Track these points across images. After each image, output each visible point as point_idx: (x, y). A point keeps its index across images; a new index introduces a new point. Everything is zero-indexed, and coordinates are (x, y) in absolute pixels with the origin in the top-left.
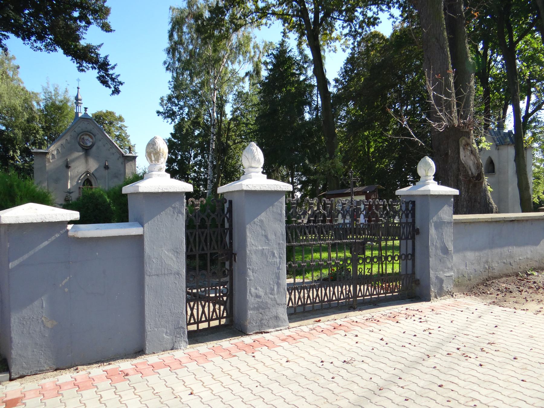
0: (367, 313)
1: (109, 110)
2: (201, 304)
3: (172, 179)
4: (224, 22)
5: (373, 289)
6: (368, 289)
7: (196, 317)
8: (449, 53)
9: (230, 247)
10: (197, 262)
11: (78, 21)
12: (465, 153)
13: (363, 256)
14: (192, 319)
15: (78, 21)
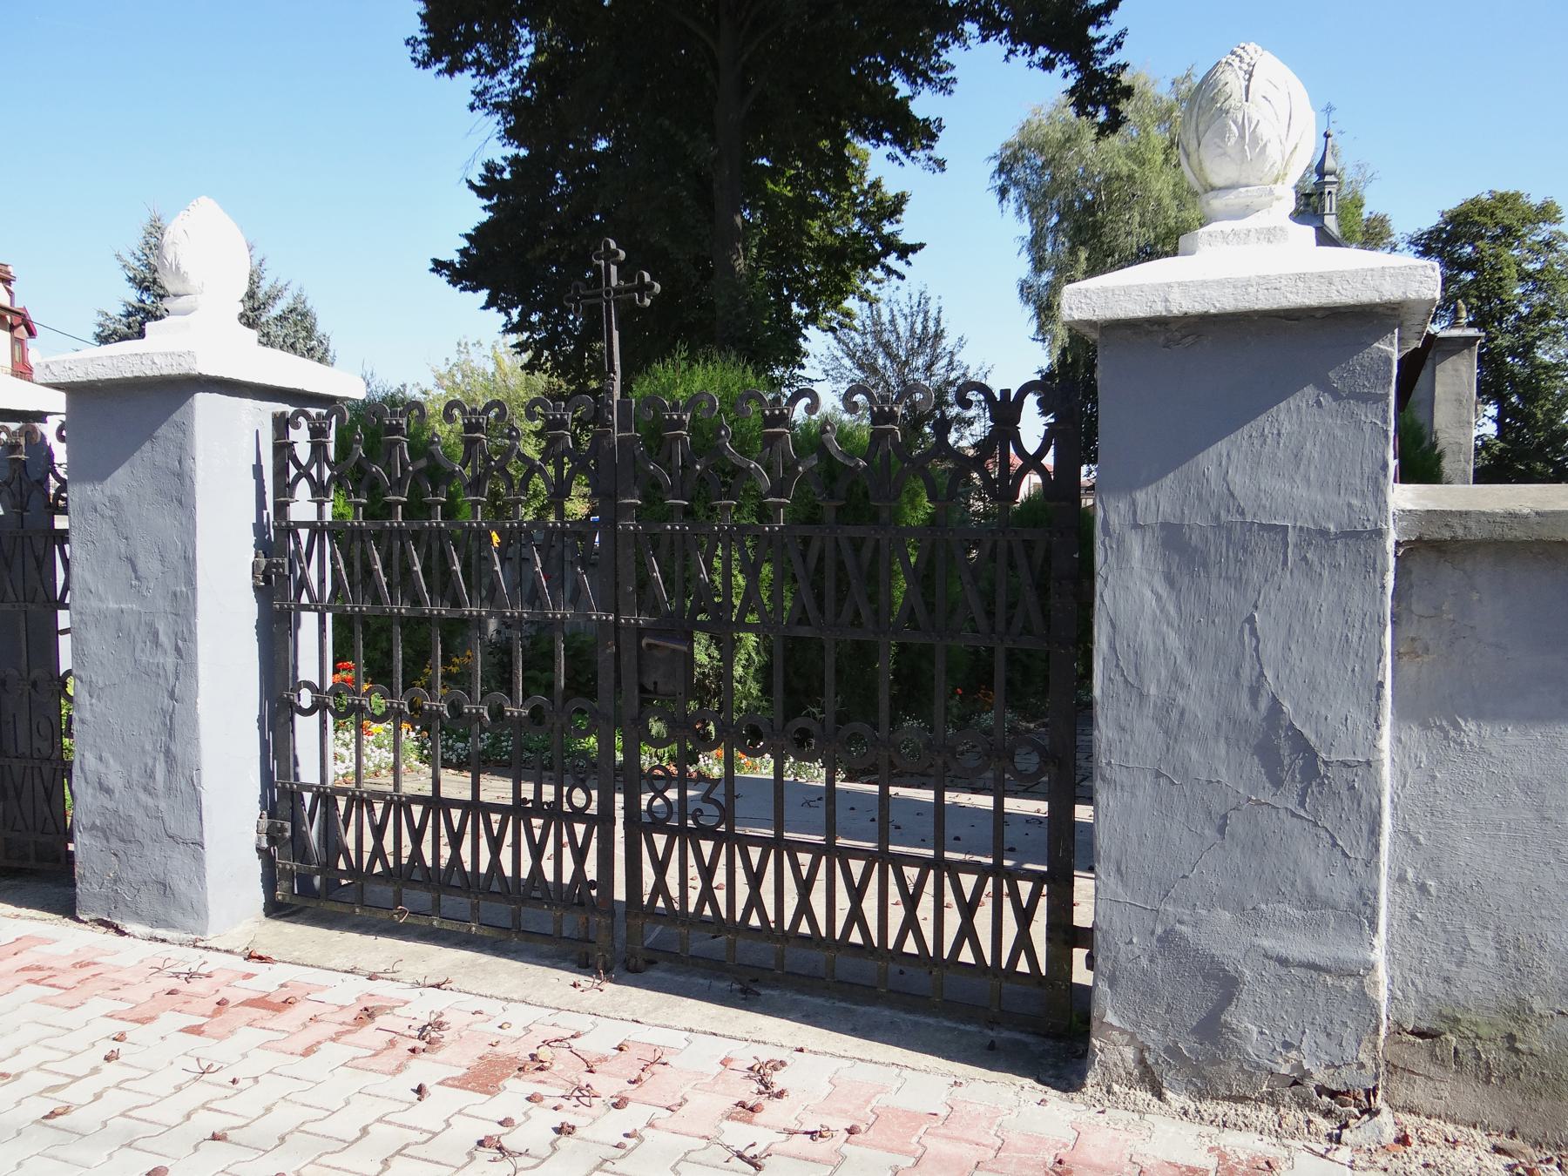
1: (1501, 189)
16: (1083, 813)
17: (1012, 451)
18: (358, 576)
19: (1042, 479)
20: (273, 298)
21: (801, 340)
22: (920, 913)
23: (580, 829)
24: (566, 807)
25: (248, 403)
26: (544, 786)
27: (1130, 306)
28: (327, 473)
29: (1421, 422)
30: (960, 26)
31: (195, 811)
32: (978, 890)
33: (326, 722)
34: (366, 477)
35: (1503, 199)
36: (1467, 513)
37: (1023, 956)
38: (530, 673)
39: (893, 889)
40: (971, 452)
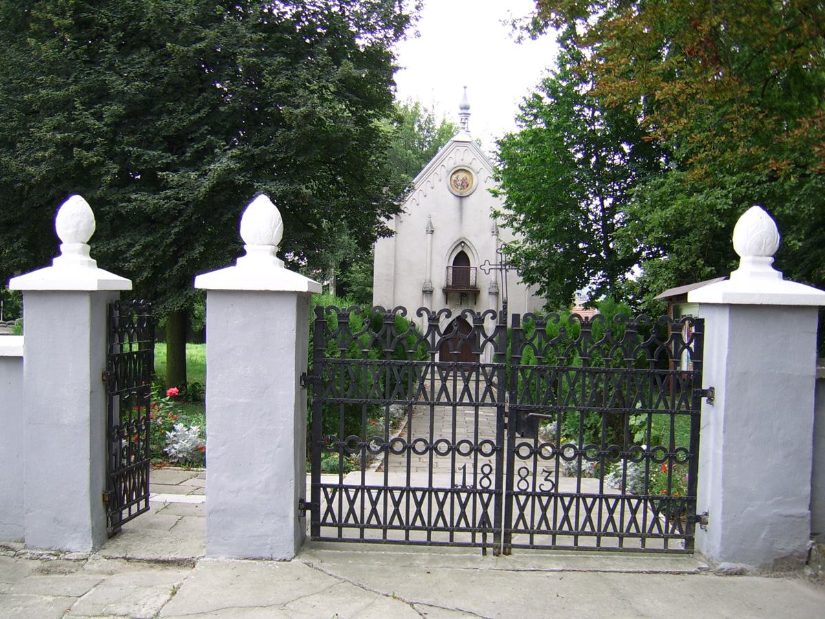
0: (372, 538)
2: (463, 376)
3: (787, 282)
4: (326, 457)
5: (671, 526)
6: (656, 520)
7: (618, 525)
8: (399, 553)
9: (450, 526)
10: (18, 333)
11: (596, 300)
12: (583, 304)
13: (531, 441)
14: (567, 504)
15: (596, 300)
16: (192, 350)
17: (436, 334)
18: (123, 375)
19: (64, 197)
20: (379, 469)
21: (500, 152)
22: (525, 513)
23: (486, 496)
24: (479, 487)
25: (582, 485)
26: (188, 345)
27: (291, 548)
28: (438, 338)
29: (598, 19)
30: (149, 276)
31: (12, 332)
32: (571, 503)
33: (605, 528)
34: (656, 376)
35: (288, 268)
36: (372, 274)
37: (463, 520)
38: (499, 529)
39: (618, 525)
40: (362, 50)
